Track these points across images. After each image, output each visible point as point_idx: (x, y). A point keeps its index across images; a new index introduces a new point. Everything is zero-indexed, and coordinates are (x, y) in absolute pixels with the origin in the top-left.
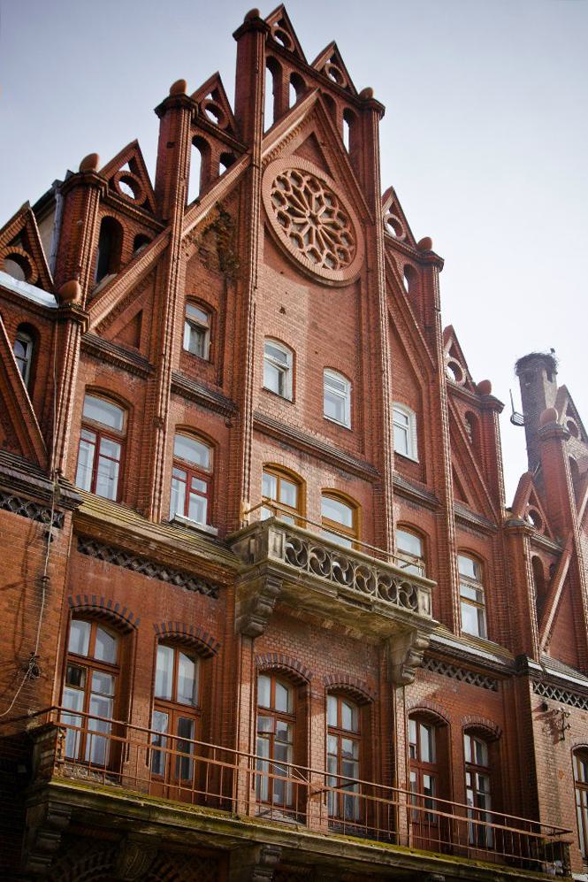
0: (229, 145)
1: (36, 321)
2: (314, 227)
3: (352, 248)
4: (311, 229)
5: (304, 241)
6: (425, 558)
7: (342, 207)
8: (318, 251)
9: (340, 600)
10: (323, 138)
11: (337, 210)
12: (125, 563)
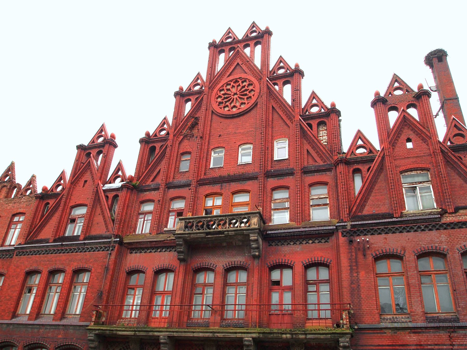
0: (198, 94)
2: (238, 95)
3: (247, 80)
4: (238, 97)
5: (243, 101)
8: (247, 96)
11: (232, 84)
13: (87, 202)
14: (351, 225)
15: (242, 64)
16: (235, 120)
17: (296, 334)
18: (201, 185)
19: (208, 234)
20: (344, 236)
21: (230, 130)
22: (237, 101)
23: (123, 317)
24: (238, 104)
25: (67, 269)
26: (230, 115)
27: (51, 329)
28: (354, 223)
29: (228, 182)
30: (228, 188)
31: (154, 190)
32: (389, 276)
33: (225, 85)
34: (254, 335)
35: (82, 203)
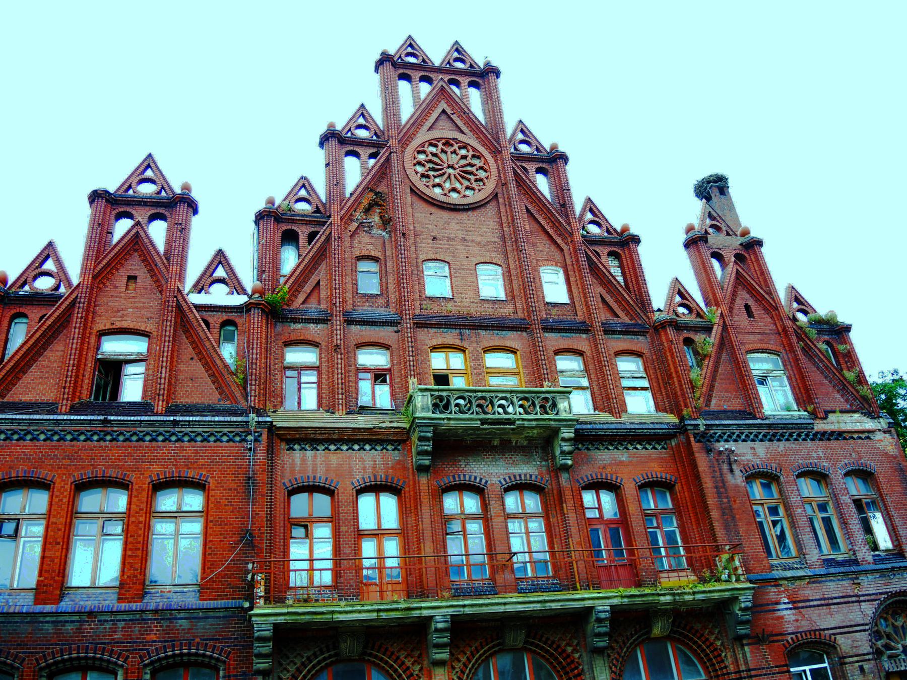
0: (374, 147)
1: (233, 316)
4: (454, 175)
5: (458, 186)
6: (587, 369)
7: (474, 149)
9: (485, 426)
10: (452, 110)
12: (323, 447)
13: (149, 327)
14: (706, 425)
15: (452, 114)
16: (463, 216)
17: (679, 594)
18: (419, 327)
19: (484, 422)
20: (699, 441)
21: (454, 232)
22: (448, 181)
23: (292, 585)
24: (447, 185)
25: (133, 477)
26: (450, 204)
27: (119, 620)
28: (708, 422)
29: (473, 329)
30: (474, 339)
31: (313, 323)
32: (176, 517)
33: (443, 141)
34: (615, 601)
35: (131, 326)
